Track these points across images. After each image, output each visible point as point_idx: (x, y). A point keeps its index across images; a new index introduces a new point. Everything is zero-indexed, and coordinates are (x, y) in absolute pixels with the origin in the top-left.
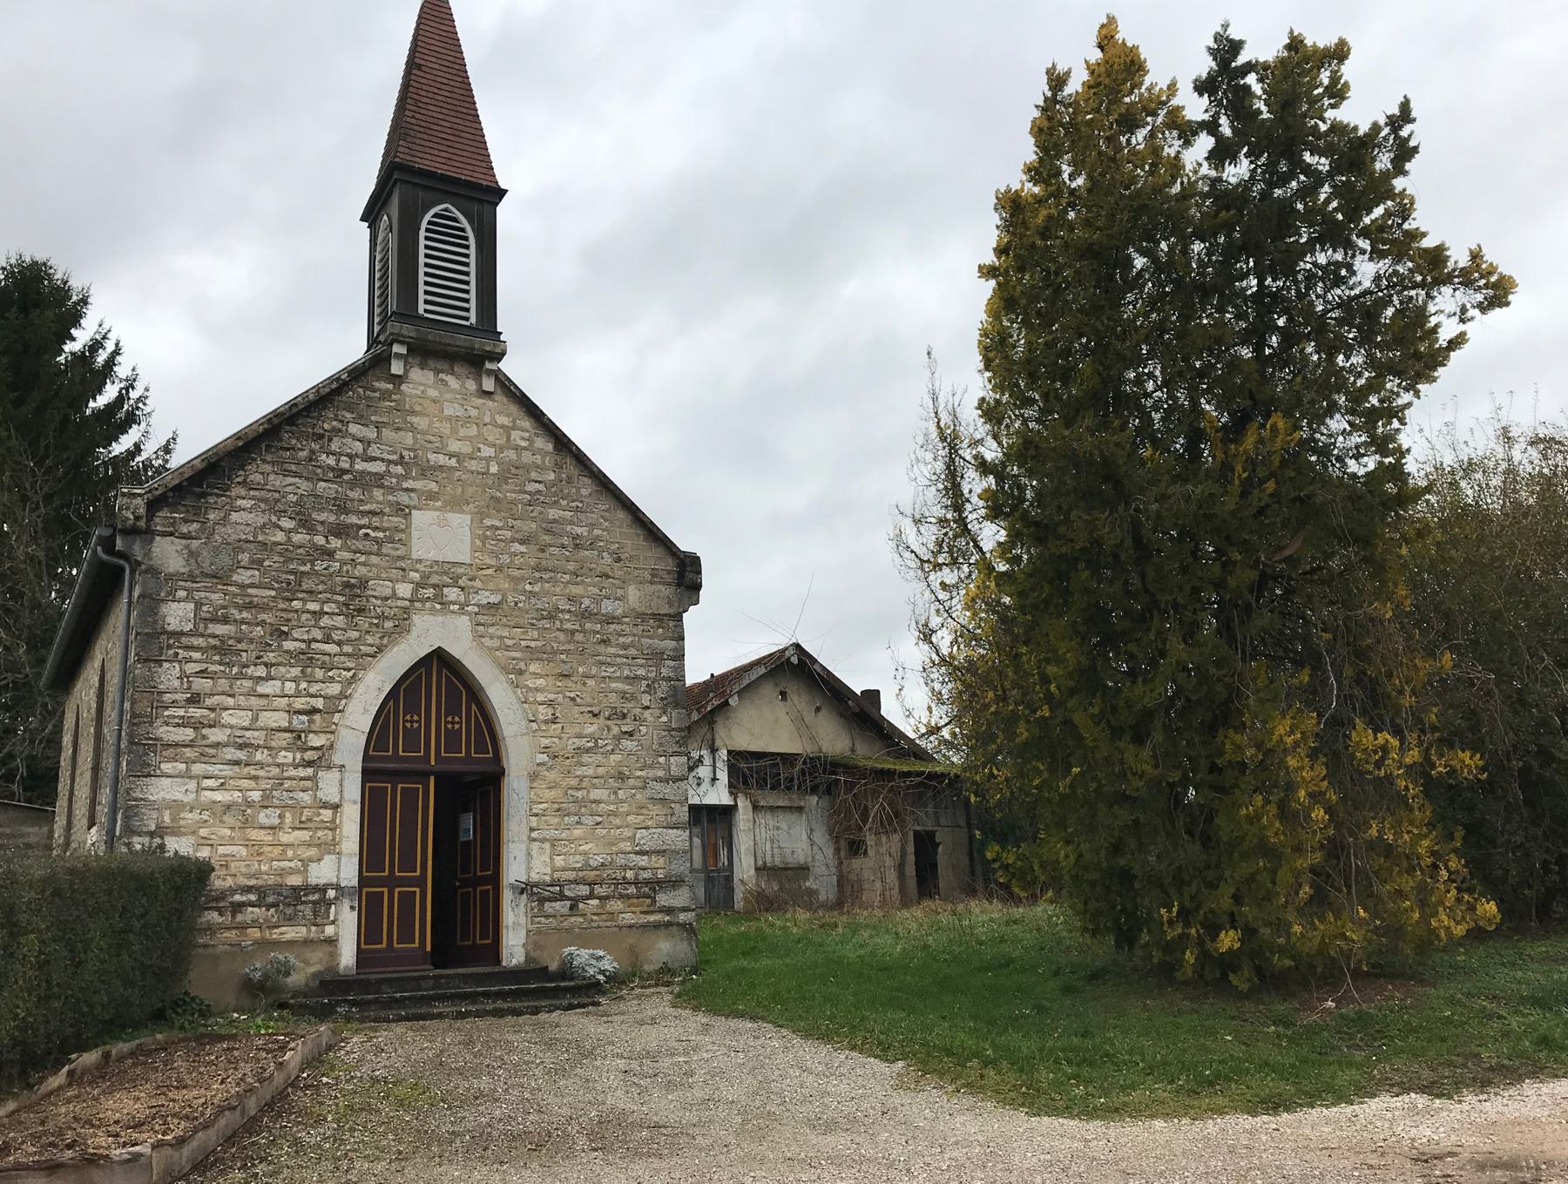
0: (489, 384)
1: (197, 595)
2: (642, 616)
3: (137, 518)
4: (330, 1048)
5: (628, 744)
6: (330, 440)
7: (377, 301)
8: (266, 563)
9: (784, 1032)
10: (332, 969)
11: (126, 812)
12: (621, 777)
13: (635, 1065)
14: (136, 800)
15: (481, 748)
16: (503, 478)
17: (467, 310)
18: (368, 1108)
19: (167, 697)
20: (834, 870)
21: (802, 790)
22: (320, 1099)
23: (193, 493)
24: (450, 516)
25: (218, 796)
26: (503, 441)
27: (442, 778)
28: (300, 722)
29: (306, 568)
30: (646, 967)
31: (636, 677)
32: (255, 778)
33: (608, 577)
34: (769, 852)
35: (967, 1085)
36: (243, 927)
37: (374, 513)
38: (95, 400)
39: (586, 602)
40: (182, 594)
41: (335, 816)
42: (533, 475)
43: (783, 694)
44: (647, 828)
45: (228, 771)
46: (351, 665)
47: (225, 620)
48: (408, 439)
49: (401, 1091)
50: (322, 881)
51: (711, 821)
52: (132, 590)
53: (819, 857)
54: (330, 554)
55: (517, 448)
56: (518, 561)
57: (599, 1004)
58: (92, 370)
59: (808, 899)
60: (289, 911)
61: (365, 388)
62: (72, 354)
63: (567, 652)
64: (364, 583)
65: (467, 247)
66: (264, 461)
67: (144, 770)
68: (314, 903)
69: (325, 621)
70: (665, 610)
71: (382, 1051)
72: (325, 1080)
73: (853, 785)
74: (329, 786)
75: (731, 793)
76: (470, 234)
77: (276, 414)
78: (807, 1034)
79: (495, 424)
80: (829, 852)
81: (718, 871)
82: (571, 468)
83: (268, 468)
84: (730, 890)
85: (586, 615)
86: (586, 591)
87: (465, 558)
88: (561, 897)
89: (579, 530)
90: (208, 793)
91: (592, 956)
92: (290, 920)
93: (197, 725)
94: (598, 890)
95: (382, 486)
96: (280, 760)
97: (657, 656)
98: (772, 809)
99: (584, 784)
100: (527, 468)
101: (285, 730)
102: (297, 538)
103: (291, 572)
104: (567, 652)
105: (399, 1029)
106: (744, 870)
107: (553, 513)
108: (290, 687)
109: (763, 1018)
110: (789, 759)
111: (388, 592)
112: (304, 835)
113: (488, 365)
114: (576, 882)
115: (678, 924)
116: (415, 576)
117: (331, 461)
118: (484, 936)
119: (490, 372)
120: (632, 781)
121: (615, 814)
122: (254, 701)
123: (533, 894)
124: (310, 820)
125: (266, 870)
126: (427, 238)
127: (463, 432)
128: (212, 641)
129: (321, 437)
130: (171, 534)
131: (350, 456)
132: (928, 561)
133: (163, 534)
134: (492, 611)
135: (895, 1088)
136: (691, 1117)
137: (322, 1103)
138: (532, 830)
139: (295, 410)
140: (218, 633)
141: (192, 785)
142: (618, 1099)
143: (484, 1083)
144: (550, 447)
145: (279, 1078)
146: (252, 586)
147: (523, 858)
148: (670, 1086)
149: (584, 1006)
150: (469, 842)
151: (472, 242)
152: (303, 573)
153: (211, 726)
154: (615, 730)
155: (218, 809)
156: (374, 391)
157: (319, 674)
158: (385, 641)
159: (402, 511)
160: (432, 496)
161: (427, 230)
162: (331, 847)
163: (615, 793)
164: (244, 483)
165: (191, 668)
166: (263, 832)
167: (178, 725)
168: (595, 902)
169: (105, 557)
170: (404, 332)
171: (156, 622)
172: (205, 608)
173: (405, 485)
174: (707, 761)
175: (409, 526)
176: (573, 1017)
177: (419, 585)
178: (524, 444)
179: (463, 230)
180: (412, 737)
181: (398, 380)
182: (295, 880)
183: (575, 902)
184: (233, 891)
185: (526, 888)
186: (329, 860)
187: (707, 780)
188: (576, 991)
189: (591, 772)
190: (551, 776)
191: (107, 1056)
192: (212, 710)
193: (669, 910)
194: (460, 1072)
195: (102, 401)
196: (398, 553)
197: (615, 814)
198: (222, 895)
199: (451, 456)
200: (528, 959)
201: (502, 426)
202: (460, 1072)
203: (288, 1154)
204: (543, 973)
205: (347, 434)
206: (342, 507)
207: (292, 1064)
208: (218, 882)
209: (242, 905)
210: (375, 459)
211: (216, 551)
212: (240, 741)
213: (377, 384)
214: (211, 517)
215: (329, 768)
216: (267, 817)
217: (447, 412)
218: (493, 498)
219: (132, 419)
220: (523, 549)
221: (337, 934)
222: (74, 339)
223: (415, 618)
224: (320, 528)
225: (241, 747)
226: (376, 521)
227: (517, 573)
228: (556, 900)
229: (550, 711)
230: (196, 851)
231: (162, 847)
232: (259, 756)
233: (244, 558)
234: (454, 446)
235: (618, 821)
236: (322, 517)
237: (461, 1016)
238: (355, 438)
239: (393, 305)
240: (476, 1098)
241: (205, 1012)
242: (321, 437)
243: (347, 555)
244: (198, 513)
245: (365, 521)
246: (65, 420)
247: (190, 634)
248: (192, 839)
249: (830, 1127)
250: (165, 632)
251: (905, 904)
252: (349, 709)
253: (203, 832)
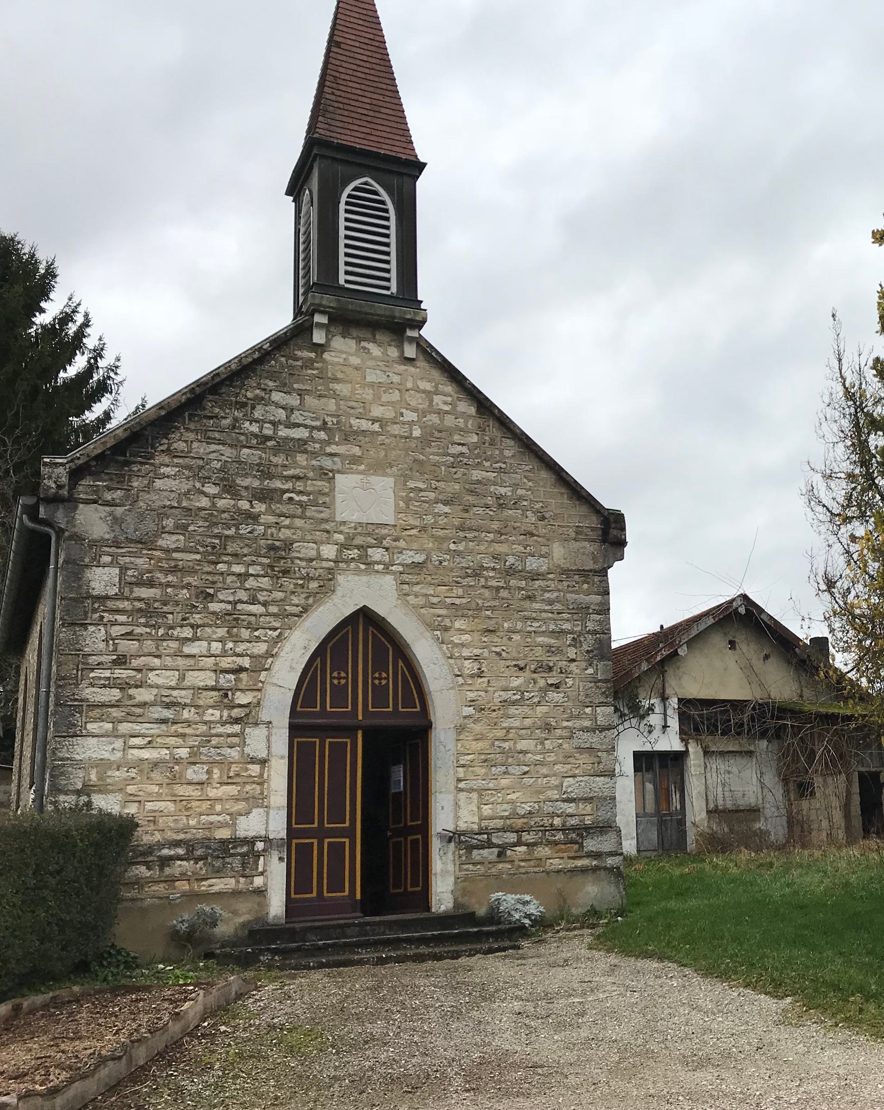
0: (410, 351)
1: (122, 560)
2: (566, 572)
3: (60, 487)
4: (240, 996)
5: (553, 696)
6: (253, 408)
7: (301, 273)
8: (191, 528)
9: (687, 971)
10: (261, 919)
11: (50, 772)
12: (548, 728)
13: (530, 1007)
14: (62, 759)
15: (408, 701)
16: (425, 441)
17: (388, 280)
18: (259, 1056)
19: (93, 660)
20: (783, 811)
21: (752, 737)
22: (213, 1047)
23: (117, 462)
24: (373, 479)
25: (146, 754)
26: (425, 406)
27: (373, 735)
28: (228, 680)
29: (232, 532)
30: (574, 911)
31: (562, 632)
32: (183, 736)
33: (532, 535)
34: (720, 796)
35: (846, 1019)
36: (171, 881)
37: (298, 478)
38: (65, 370)
39: (511, 560)
40: (106, 559)
41: (262, 769)
42: (456, 438)
43: (732, 644)
44: (574, 776)
45: (155, 729)
46: (277, 624)
47: (151, 584)
48: (331, 405)
49: (293, 1039)
50: (251, 834)
51: (663, 766)
52: (58, 556)
53: (769, 797)
54: (254, 518)
55: (439, 412)
56: (442, 521)
57: (518, 948)
58: (64, 340)
59: (757, 841)
60: (218, 863)
61: (288, 358)
62: (43, 327)
63: (492, 608)
64: (288, 545)
65: (387, 219)
66: (187, 429)
67: (71, 731)
68: (243, 855)
69: (251, 583)
70: (590, 565)
71: (286, 999)
72: (223, 1028)
73: (800, 729)
74: (256, 741)
75: (682, 740)
76: (390, 206)
77: (198, 383)
78: (708, 972)
79: (418, 390)
80: (779, 792)
81: (670, 815)
82: (493, 430)
83: (191, 436)
84: (683, 833)
85: (510, 572)
86: (511, 550)
87: (389, 518)
88: (489, 845)
89: (503, 491)
90: (135, 752)
91: (519, 901)
92: (218, 872)
93: (124, 686)
94: (526, 837)
95: (305, 452)
96: (207, 718)
97: (582, 611)
98: (722, 754)
99: (511, 736)
100: (450, 431)
101: (213, 689)
102: (221, 503)
103: (216, 536)
104: (492, 608)
105: (316, 975)
106: (696, 813)
107: (477, 475)
108: (216, 647)
109: (670, 959)
110: (737, 705)
111: (313, 553)
112: (232, 790)
113: (410, 333)
114: (504, 830)
115: (605, 868)
116: (340, 538)
117: (255, 428)
118: (415, 884)
119: (411, 340)
120: (558, 732)
121: (541, 763)
122: (181, 662)
123: (460, 842)
124: (238, 775)
125: (194, 825)
126: (347, 211)
127: (385, 398)
128: (138, 605)
129: (244, 405)
130: (95, 502)
131: (273, 423)
132: (839, 515)
133: (87, 502)
134: (417, 570)
135: (777, 1024)
136: (571, 1056)
137: (213, 1052)
138: (459, 780)
139: (217, 380)
140: (143, 596)
141: (119, 744)
142: (507, 1040)
143: (377, 1028)
144: (472, 410)
145: (175, 1028)
146: (177, 550)
147: (451, 809)
148: (560, 1026)
149: (504, 949)
150: (400, 793)
151: (392, 214)
152: (227, 536)
153: (137, 687)
154: (542, 683)
155: (146, 766)
156: (297, 360)
157: (245, 634)
158: (311, 601)
159: (326, 475)
160: (355, 460)
161: (347, 203)
162: (259, 801)
163: (542, 743)
164: (168, 452)
165: (116, 631)
166: (192, 787)
167: (105, 686)
168: (523, 849)
169: (31, 525)
170: (324, 302)
171: (80, 587)
172: (130, 573)
173: (328, 450)
174: (658, 709)
175: (333, 489)
176: (476, 961)
177: (343, 547)
178: (447, 408)
179: (383, 202)
180: (339, 694)
181: (319, 348)
182: (224, 834)
183: (502, 850)
184: (161, 845)
185: (453, 837)
186: (257, 814)
187: (658, 728)
188: (498, 935)
189: (517, 724)
190: (478, 728)
191: (17, 1009)
192: (139, 671)
193: (597, 855)
194: (358, 1018)
195: (72, 371)
196: (322, 515)
197: (541, 763)
198: (150, 849)
199: (374, 421)
200: (457, 905)
201: (424, 392)
202: (358, 1018)
203: (166, 1102)
204: (470, 918)
205: (269, 402)
206: (266, 472)
207: (191, 1014)
208: (146, 837)
209: (172, 858)
210: (298, 425)
211: (141, 517)
212: (167, 700)
213: (299, 353)
214: (135, 484)
215: (256, 724)
216: (194, 773)
217: (369, 379)
218: (415, 460)
219: (103, 388)
220: (447, 509)
221: (265, 884)
222: (42, 311)
223: (340, 579)
224: (244, 493)
225: (168, 706)
226: (300, 486)
227: (441, 533)
228: (483, 848)
229: (476, 666)
230: (123, 807)
231: (89, 804)
232: (186, 714)
233: (169, 523)
234: (377, 411)
235: (544, 771)
236: (247, 482)
237: (381, 962)
238: (277, 405)
239: (314, 278)
240: (366, 1042)
241: (131, 964)
242: (244, 405)
243: (271, 519)
244: (121, 481)
245: (289, 485)
246: (35, 391)
247: (115, 597)
248: (119, 797)
249: (703, 1063)
250: (90, 596)
251: (851, 841)
252: (275, 668)
253: (131, 789)
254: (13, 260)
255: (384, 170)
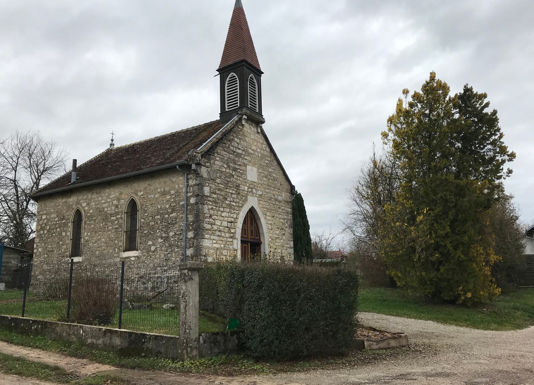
2: (285, 201)
32: (222, 241)
144: (269, 151)
159: (245, 165)
223: (249, 197)
254: (454, 166)
255: (234, 69)
